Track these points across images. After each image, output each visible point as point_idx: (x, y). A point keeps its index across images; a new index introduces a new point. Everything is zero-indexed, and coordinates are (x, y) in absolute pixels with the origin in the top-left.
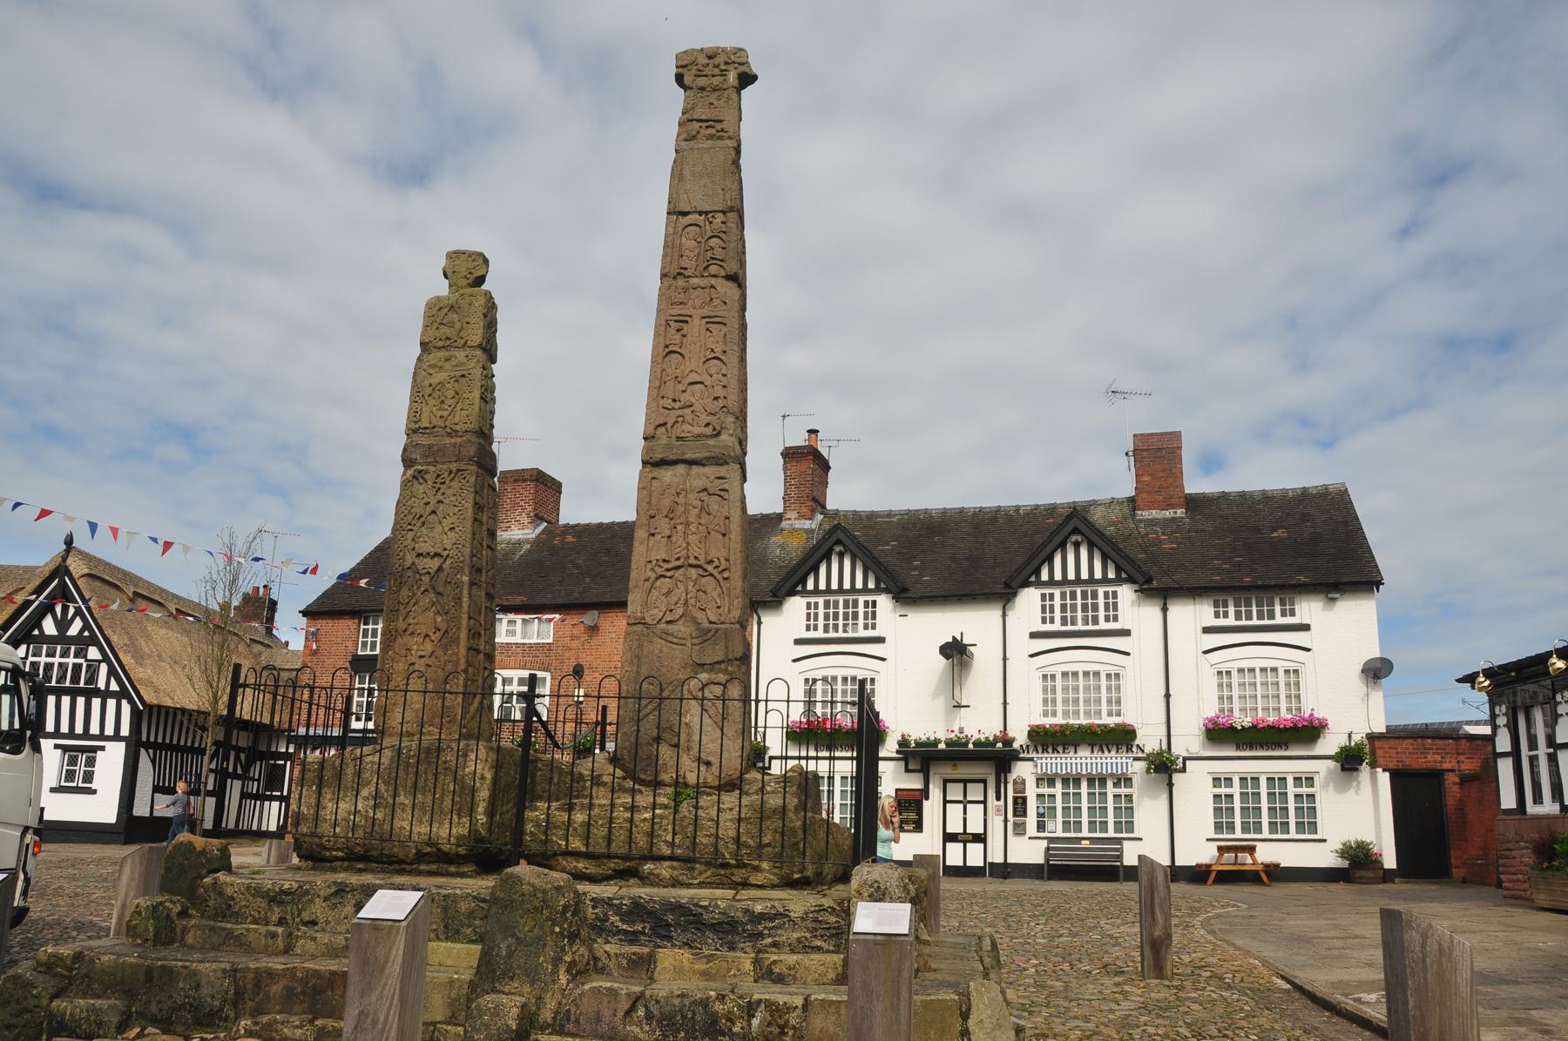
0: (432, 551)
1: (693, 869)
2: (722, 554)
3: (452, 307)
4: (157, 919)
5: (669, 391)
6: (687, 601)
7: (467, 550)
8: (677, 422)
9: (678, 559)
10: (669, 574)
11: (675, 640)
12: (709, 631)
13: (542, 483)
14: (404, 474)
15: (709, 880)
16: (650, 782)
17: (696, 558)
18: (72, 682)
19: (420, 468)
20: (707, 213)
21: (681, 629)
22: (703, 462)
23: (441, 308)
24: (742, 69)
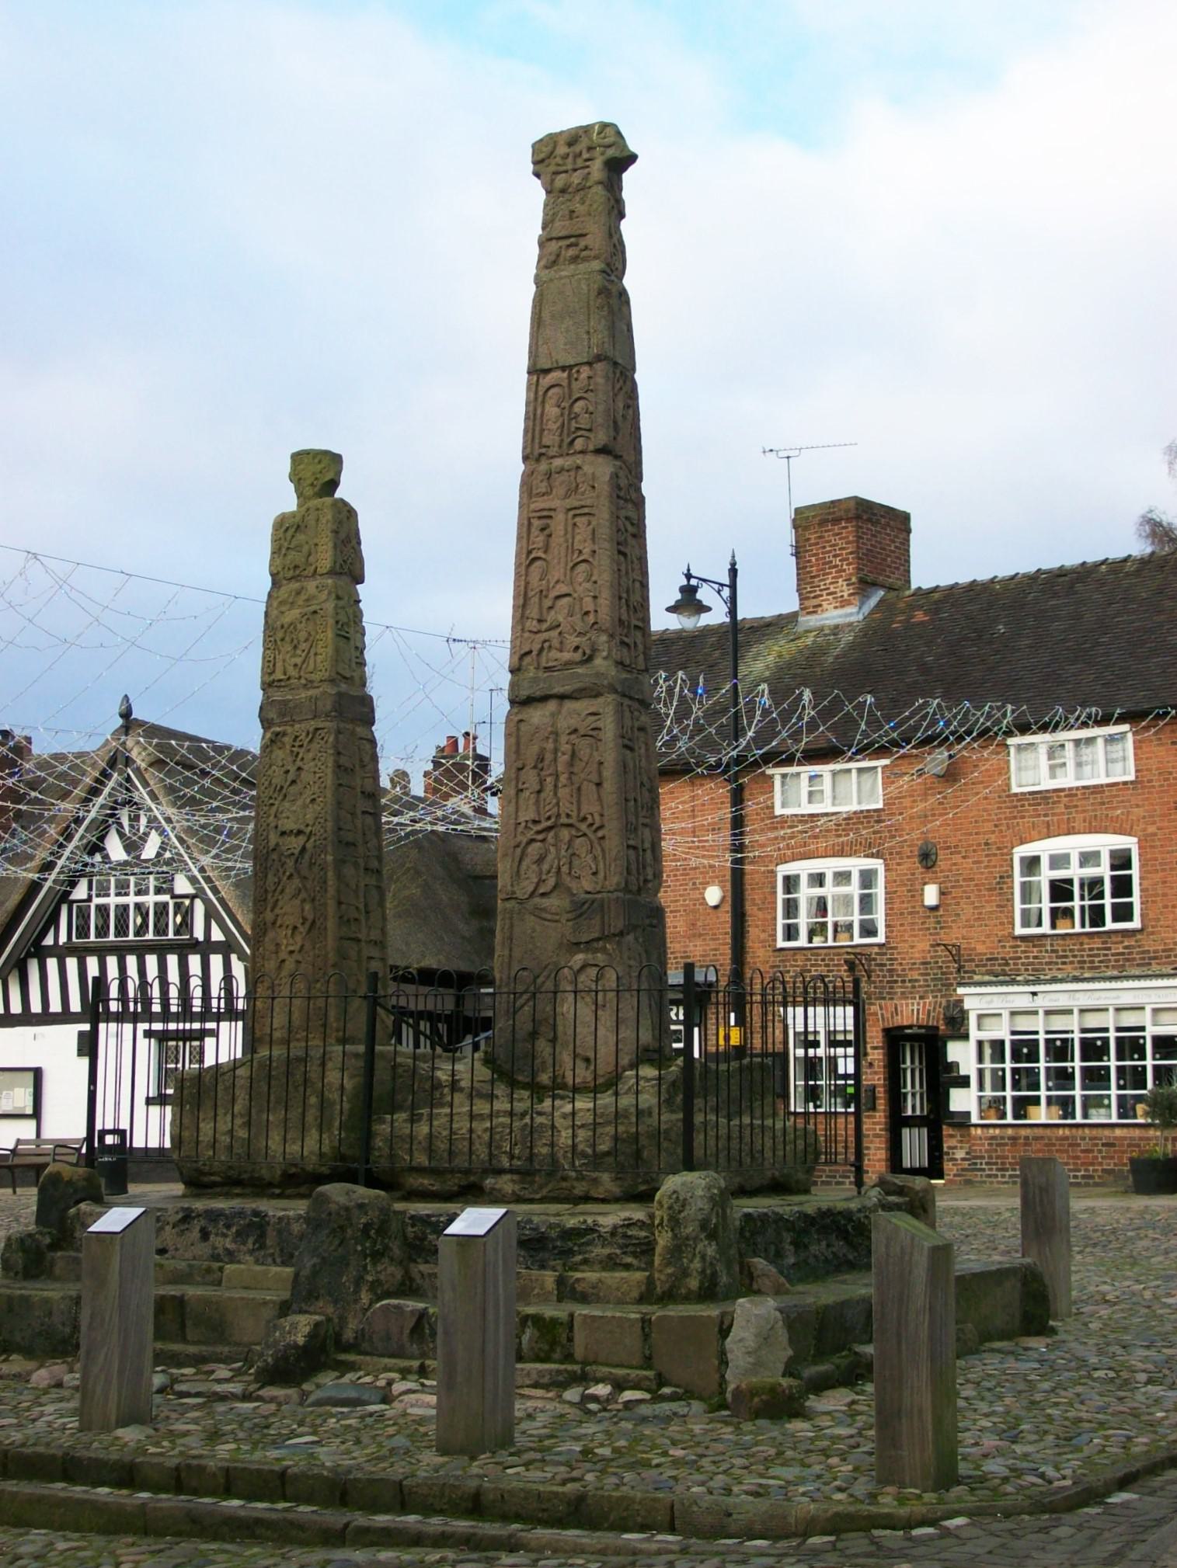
0: (295, 827)
1: (532, 1183)
2: (595, 809)
3: (298, 526)
4: (25, 1251)
5: (533, 612)
6: (559, 869)
7: (330, 824)
8: (542, 649)
9: (549, 818)
10: (540, 837)
11: (549, 917)
12: (584, 903)
13: (869, 520)
14: (263, 738)
15: (551, 1194)
16: (528, 1083)
17: (568, 816)
18: (157, 932)
19: (278, 729)
20: (571, 367)
21: (554, 902)
22: (574, 695)
23: (287, 529)
24: (611, 152)
